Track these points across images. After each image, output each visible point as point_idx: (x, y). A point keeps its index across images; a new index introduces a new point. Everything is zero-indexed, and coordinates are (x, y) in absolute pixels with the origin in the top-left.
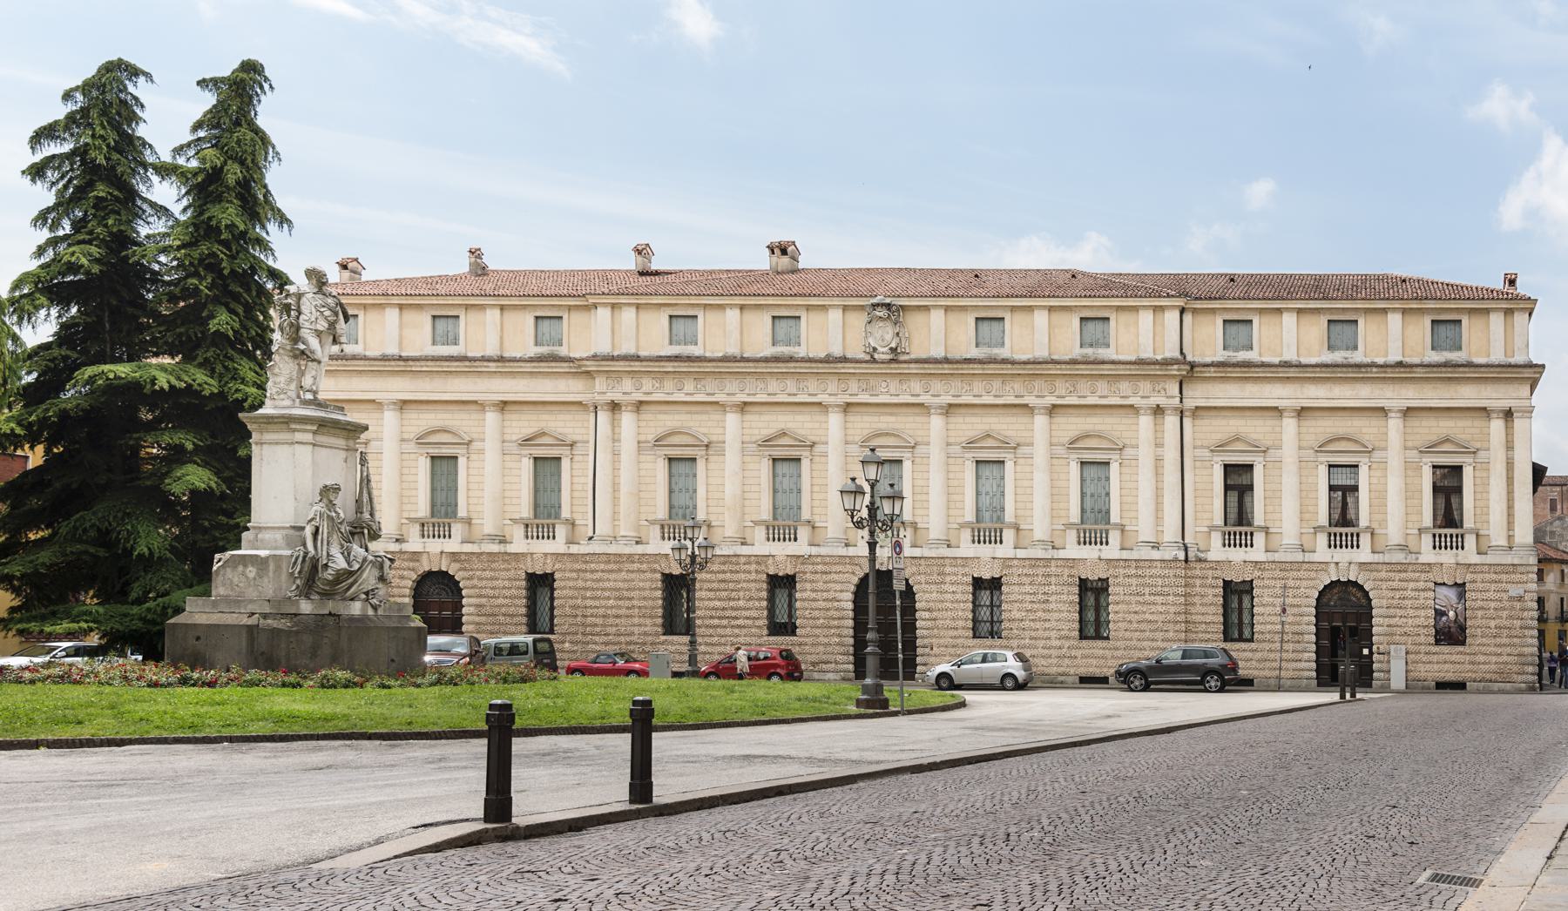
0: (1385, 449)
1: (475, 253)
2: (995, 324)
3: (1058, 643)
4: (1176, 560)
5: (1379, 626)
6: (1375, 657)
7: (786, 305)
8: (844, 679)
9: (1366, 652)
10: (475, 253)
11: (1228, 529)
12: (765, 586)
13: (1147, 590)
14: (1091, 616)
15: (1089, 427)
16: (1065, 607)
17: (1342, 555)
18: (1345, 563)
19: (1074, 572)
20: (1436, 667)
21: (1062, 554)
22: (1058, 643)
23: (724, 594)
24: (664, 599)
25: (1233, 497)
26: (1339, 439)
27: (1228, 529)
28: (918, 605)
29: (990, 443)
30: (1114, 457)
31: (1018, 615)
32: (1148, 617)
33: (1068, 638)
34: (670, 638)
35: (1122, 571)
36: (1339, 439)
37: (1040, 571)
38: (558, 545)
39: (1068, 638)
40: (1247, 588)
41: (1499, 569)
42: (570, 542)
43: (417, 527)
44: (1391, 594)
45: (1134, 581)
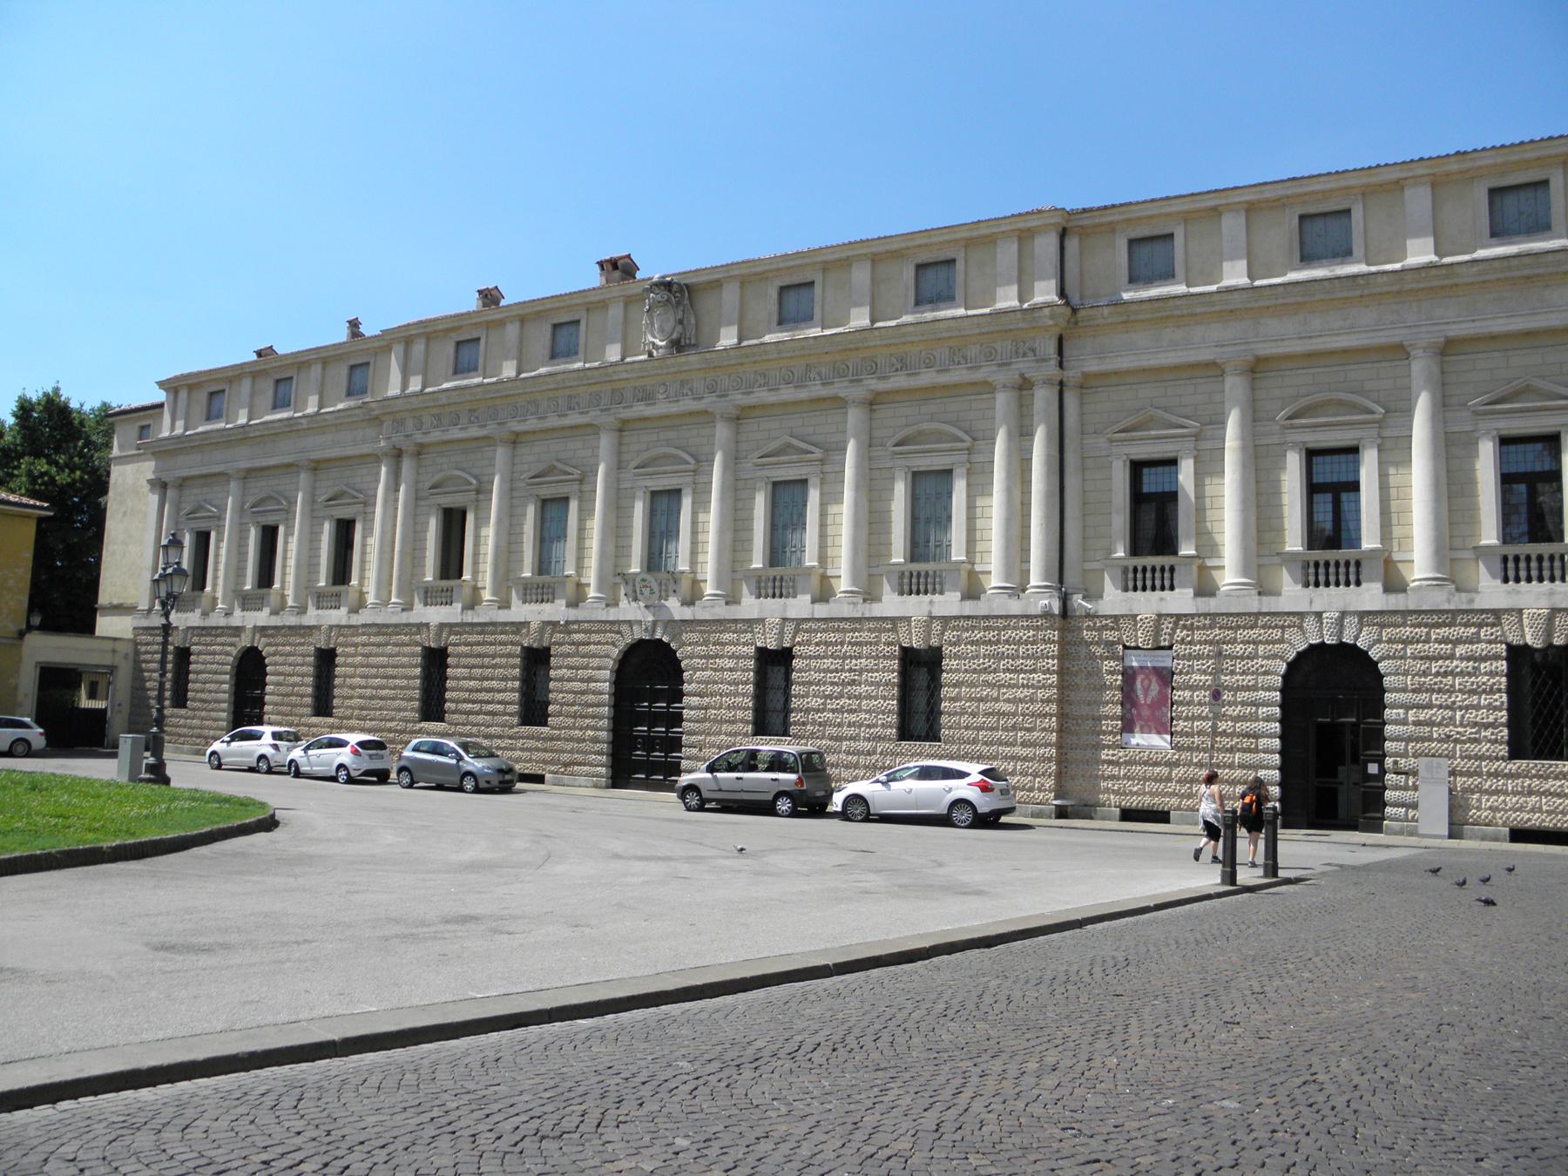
1: (354, 324)
2: (803, 291)
3: (868, 746)
4: (1047, 615)
5: (1398, 722)
7: (492, 315)
8: (596, 786)
9: (1373, 768)
10: (354, 324)
11: (1511, 550)
12: (751, 663)
14: (920, 701)
17: (1331, 599)
18: (1331, 611)
20: (1512, 800)
22: (868, 746)
23: (368, 692)
25: (1324, 503)
27: (1511, 550)
31: (815, 702)
33: (879, 738)
39: (879, 738)
41: (1234, 621)
44: (1421, 666)
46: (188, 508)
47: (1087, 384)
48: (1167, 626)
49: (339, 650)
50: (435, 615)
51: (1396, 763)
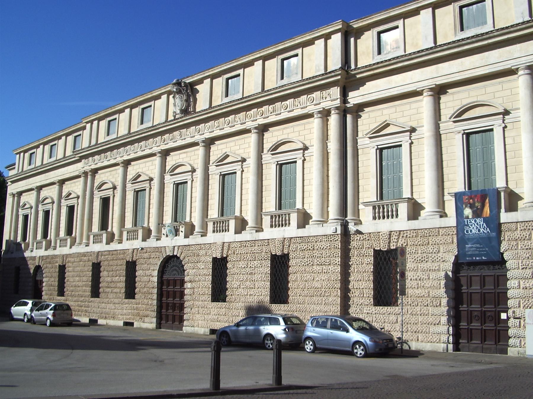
6: (511, 322)
9: (503, 316)
21: (261, 236)
30: (496, 123)
34: (379, 308)
47: (360, 107)
48: (394, 237)
51: (514, 312)
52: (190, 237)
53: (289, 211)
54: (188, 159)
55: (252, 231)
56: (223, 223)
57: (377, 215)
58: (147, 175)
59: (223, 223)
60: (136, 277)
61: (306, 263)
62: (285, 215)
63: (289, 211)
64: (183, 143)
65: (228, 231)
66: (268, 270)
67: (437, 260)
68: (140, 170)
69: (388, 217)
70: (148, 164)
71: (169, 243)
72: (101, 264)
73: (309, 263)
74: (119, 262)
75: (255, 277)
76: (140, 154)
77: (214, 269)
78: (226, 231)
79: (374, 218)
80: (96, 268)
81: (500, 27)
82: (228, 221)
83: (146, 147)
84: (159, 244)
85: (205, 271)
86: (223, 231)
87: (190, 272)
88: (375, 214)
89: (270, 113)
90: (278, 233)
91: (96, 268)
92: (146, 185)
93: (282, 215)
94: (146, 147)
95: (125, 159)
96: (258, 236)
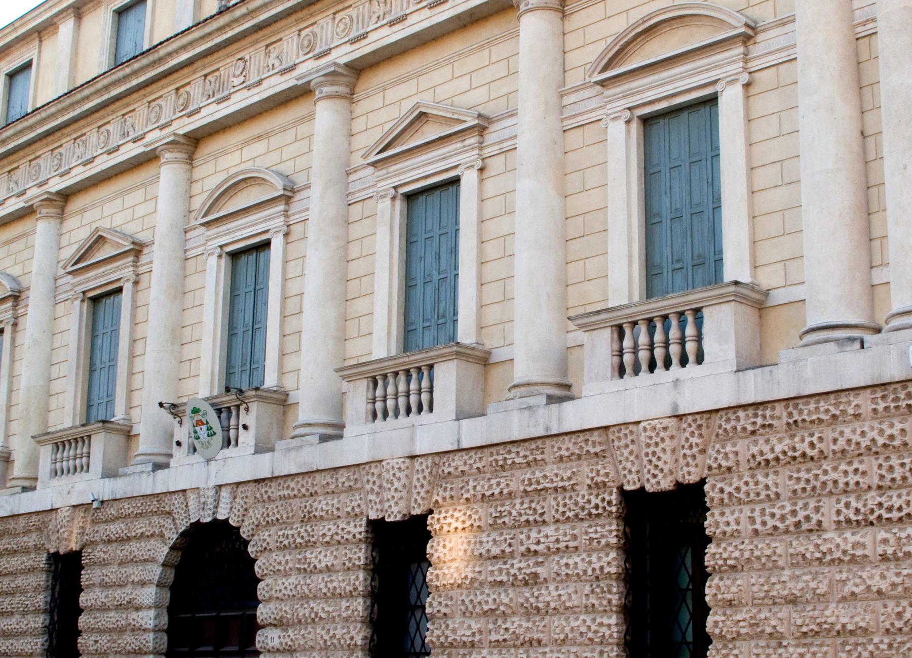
0: (512, 114)
12: (360, 555)
13: (829, 510)
15: (408, 105)
16: (575, 595)
19: (605, 470)
21: (573, 416)
24: (50, 612)
26: (650, 31)
28: (263, 612)
29: (430, 132)
30: (722, 71)
32: (839, 615)
35: (744, 448)
36: (650, 31)
37: (516, 482)
38: (707, 385)
40: (689, 500)
42: (753, 360)
43: (604, 339)
45: (782, 481)
46: (594, 52)
49: (99, 552)
50: (647, 398)
52: (280, 445)
53: (695, 297)
54: (273, 158)
55: (531, 401)
56: (651, 333)
57: (379, 405)
58: (125, 236)
59: (651, 333)
60: (80, 611)
61: (791, 520)
62: (396, 374)
63: (695, 297)
64: (256, 99)
65: (431, 409)
66: (611, 562)
67: (805, 526)
68: (106, 224)
69: (397, 415)
70: (130, 199)
71: (205, 479)
72: (432, 523)
73: (801, 515)
74: (870, 464)
75: (548, 595)
76: (104, 163)
77: (633, 547)
78: (420, 409)
79: (621, 371)
80: (66, 571)
81: (208, 16)
82: (431, 367)
83: (124, 135)
84: (164, 482)
85: (339, 582)
86: (408, 411)
87: (277, 589)
88: (621, 354)
89: (374, 19)
90: (647, 398)
91: (66, 571)
92: (123, 271)
93: (385, 376)
94: (124, 135)
95: (54, 190)
96: (560, 420)
